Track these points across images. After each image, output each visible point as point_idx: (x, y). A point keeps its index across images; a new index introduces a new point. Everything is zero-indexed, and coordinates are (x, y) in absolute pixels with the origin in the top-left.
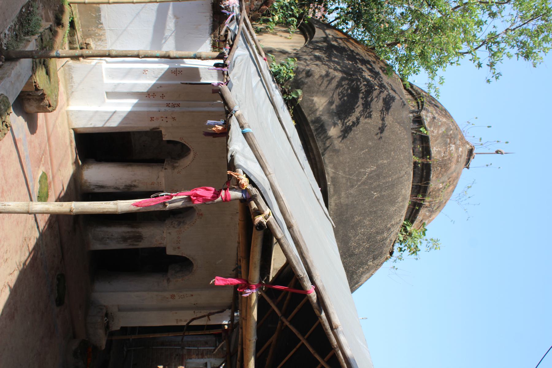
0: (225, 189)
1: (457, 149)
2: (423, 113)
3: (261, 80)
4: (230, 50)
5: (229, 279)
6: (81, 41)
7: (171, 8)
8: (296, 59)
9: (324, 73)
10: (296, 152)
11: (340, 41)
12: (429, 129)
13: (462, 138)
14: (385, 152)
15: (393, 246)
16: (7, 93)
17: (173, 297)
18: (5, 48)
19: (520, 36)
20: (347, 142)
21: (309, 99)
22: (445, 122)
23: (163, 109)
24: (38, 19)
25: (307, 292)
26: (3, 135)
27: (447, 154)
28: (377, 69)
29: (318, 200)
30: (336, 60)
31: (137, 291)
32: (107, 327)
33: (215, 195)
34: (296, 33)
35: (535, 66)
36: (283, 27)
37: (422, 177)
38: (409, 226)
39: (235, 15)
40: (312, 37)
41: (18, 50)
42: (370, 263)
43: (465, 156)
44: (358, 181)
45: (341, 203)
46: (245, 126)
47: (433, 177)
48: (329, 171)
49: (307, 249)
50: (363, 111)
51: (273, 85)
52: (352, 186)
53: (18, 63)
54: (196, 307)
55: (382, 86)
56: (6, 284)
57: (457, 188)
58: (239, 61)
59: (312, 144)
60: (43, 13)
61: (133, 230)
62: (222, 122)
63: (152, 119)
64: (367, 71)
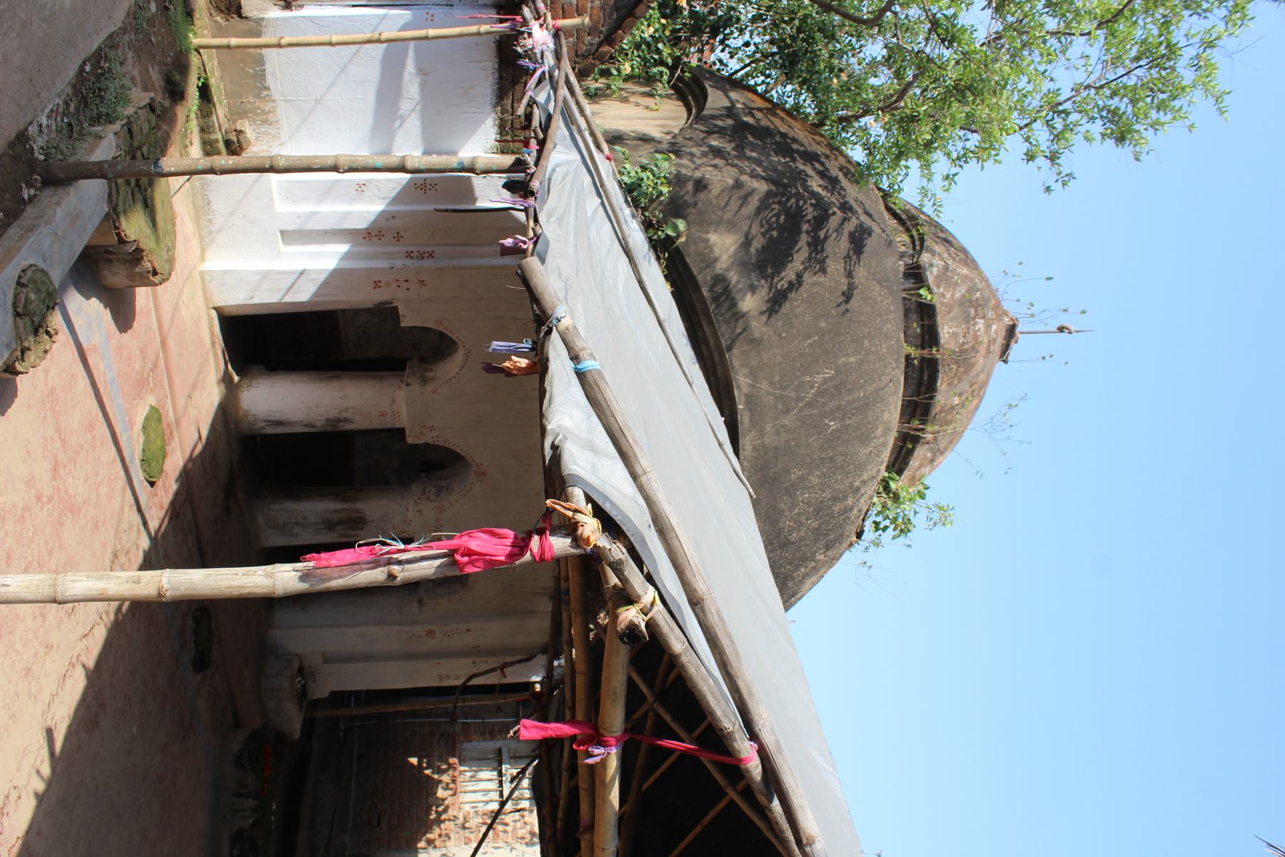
0: (541, 533)
1: (988, 327)
2: (925, 258)
3: (602, 203)
4: (540, 152)
5: (553, 725)
6: (225, 126)
7: (411, 53)
8: (673, 157)
9: (731, 182)
10: (677, 350)
11: (759, 115)
12: (935, 290)
13: (998, 306)
14: (852, 340)
15: (863, 520)
16: (45, 260)
17: (430, 634)
18: (42, 157)
19: (1111, 98)
20: (778, 322)
21: (700, 238)
22: (967, 276)
23: (399, 263)
24: (123, 86)
25: (741, 760)
26: (41, 354)
27: (970, 337)
28: (835, 172)
29: (720, 445)
30: (754, 154)
31: (359, 625)
32: (303, 693)
33: (516, 550)
34: (668, 96)
35: (1138, 160)
36: (641, 84)
37: (920, 384)
38: (893, 479)
39: (546, 69)
40: (701, 108)
41: (72, 160)
42: (820, 557)
43: (1000, 340)
44: (798, 400)
45: (763, 446)
46: (583, 354)
47: (942, 384)
48: (742, 382)
49: (737, 654)
50: (810, 258)
51: (626, 212)
52: (787, 411)
53: (72, 190)
54: (476, 652)
55: (845, 207)
56: (74, 660)
57: (984, 401)
58: (560, 179)
59: (706, 329)
60: (136, 73)
61: (347, 506)
62: (527, 345)
63: (377, 284)
64: (817, 177)
